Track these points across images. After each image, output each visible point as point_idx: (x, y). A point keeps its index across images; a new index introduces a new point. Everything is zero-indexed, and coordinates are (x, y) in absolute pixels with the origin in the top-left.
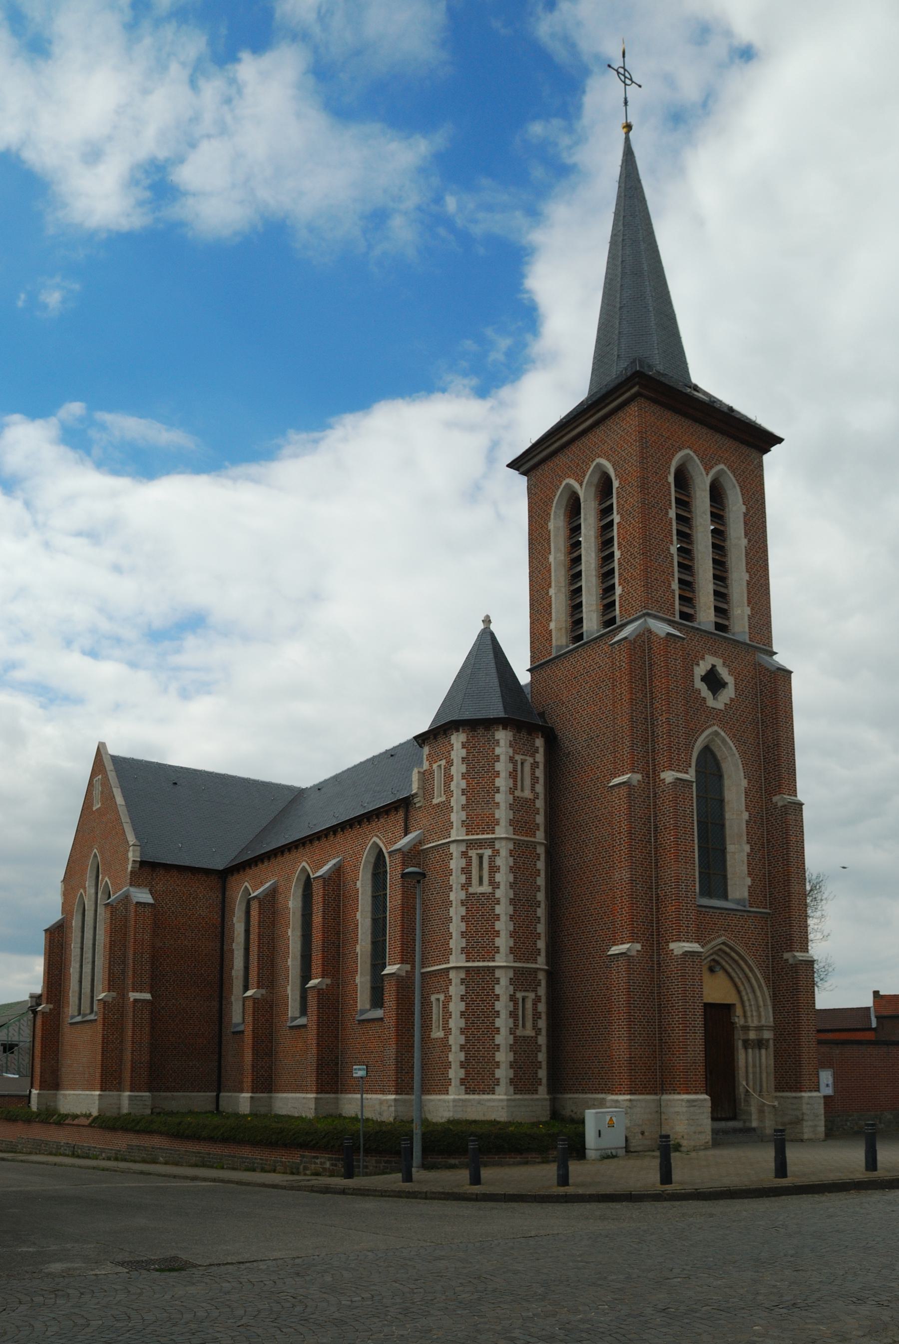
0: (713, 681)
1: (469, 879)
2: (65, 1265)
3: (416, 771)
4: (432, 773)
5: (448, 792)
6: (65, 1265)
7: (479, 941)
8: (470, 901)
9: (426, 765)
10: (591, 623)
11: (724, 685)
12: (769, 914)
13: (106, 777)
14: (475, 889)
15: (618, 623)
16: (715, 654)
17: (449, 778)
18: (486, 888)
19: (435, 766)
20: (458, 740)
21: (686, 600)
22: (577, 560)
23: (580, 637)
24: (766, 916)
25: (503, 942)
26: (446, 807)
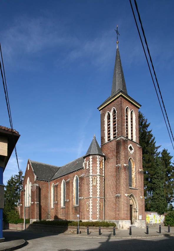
0: (131, 148)
1: (93, 182)
2: (71, 213)
3: (83, 163)
4: (86, 163)
5: (89, 167)
6: (71, 213)
7: (95, 192)
8: (93, 186)
9: (85, 162)
10: (112, 138)
11: (132, 149)
12: (19, 218)
13: (30, 164)
14: (94, 184)
15: (117, 137)
16: (131, 144)
17: (89, 164)
18: (95, 184)
19: (87, 162)
20: (91, 157)
21: (127, 134)
22: (109, 131)
23: (110, 140)
24: (18, 217)
25: (98, 193)
26: (89, 170)
